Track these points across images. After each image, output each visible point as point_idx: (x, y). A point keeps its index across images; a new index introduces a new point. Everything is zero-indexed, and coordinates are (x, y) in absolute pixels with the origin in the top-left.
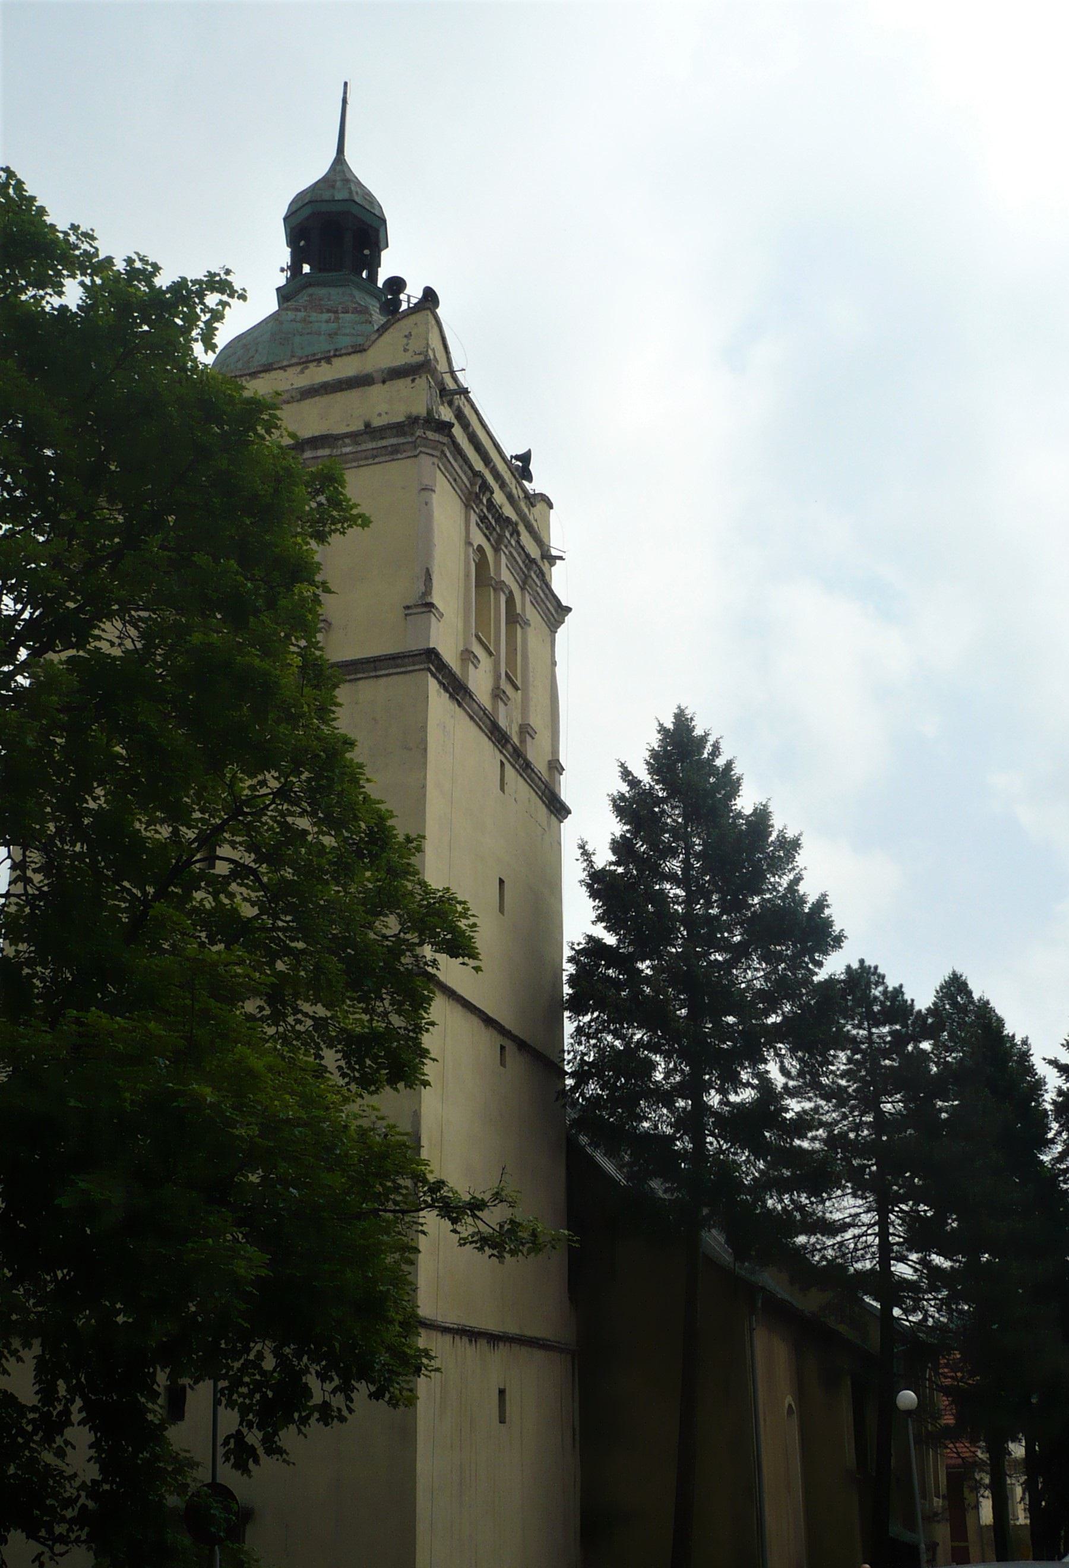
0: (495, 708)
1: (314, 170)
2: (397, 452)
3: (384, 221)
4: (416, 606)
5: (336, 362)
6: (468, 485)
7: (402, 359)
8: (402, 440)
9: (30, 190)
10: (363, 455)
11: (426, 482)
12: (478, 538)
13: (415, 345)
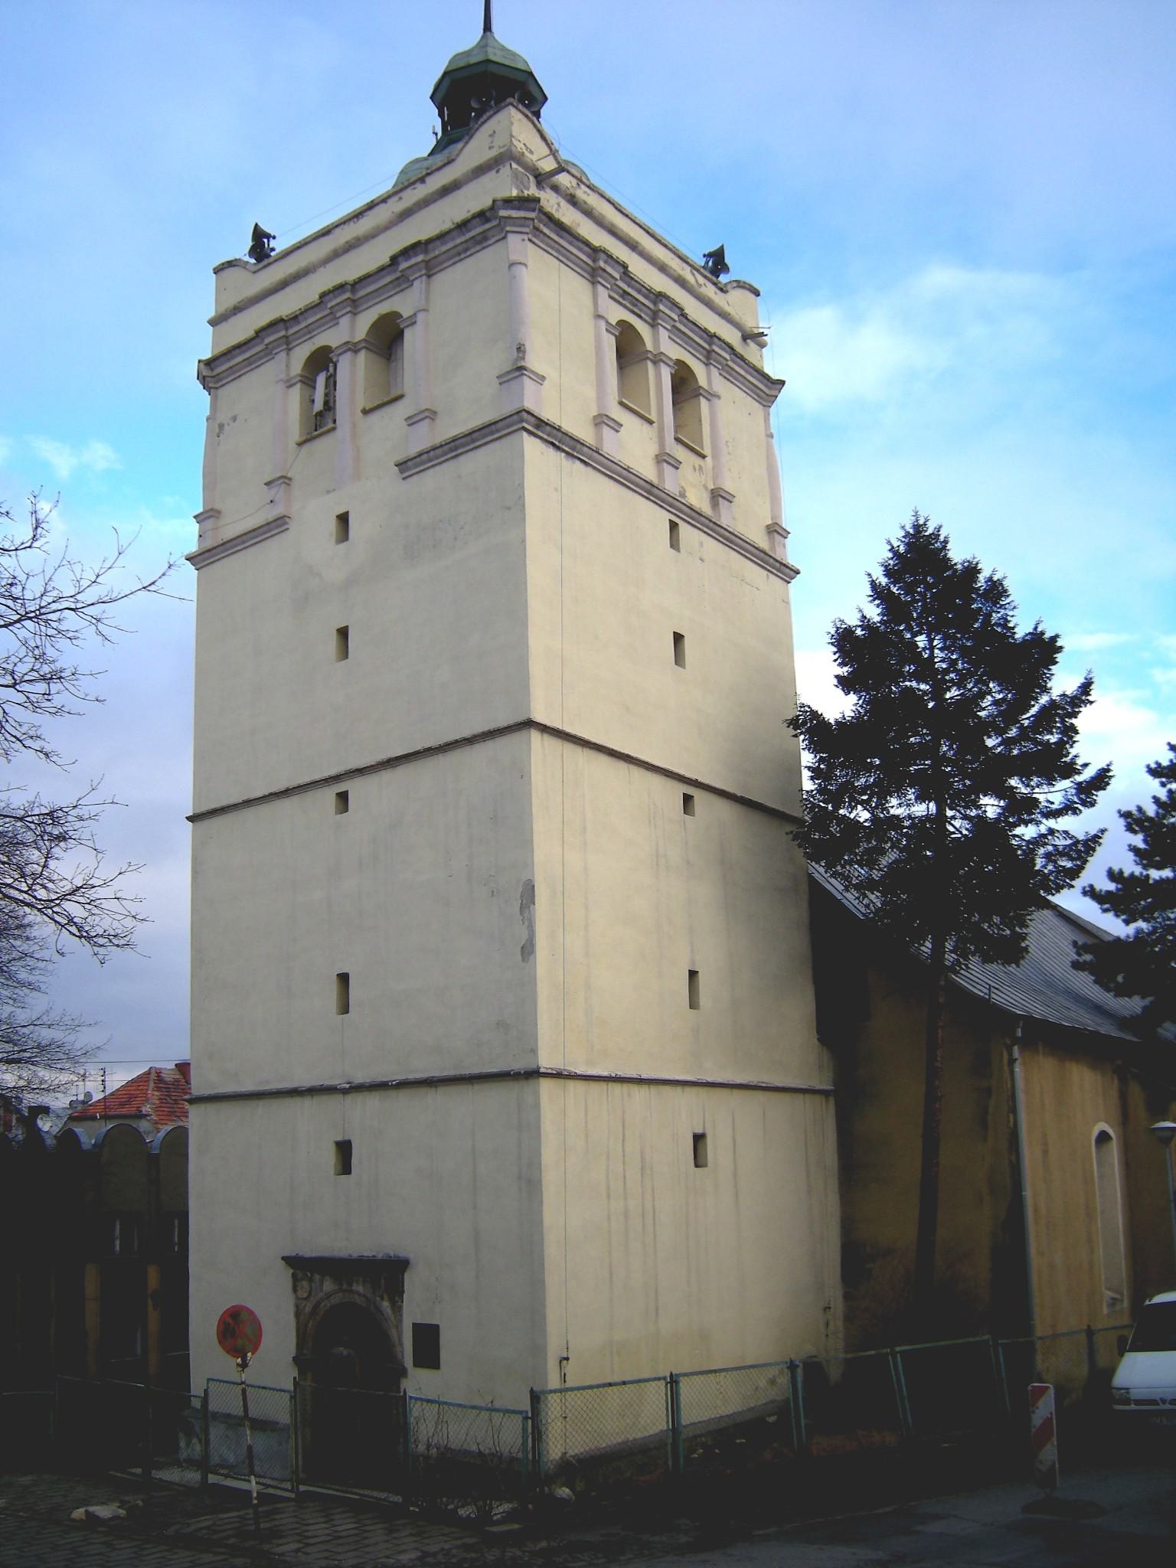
0: (599, 437)
1: (465, 38)
2: (486, 239)
3: (531, 74)
4: (508, 373)
5: (428, 180)
6: (590, 262)
7: (489, 155)
8: (488, 226)
9: (814, 708)
10: (454, 251)
11: (514, 257)
12: (617, 313)
13: (500, 141)
